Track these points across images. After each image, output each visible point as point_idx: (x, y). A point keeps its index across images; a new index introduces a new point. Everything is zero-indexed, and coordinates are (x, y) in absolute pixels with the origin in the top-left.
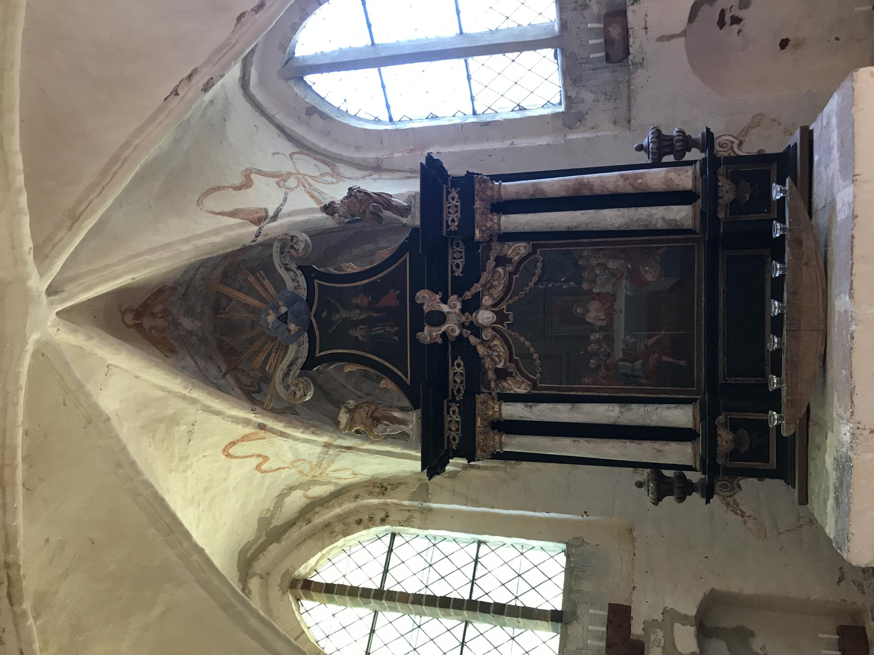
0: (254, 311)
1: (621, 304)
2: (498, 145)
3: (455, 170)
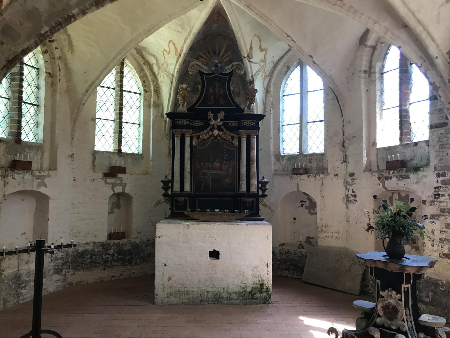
0: (219, 53)
1: (219, 172)
2: (272, 134)
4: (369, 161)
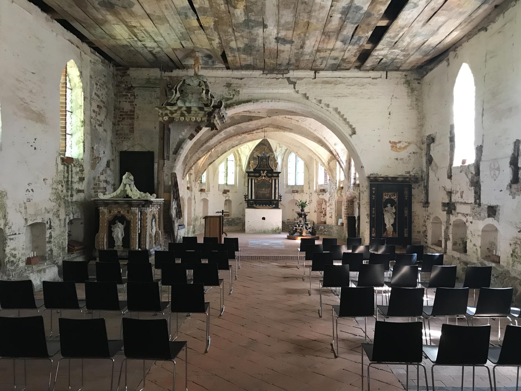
3: (280, 175)
4: (316, 189)
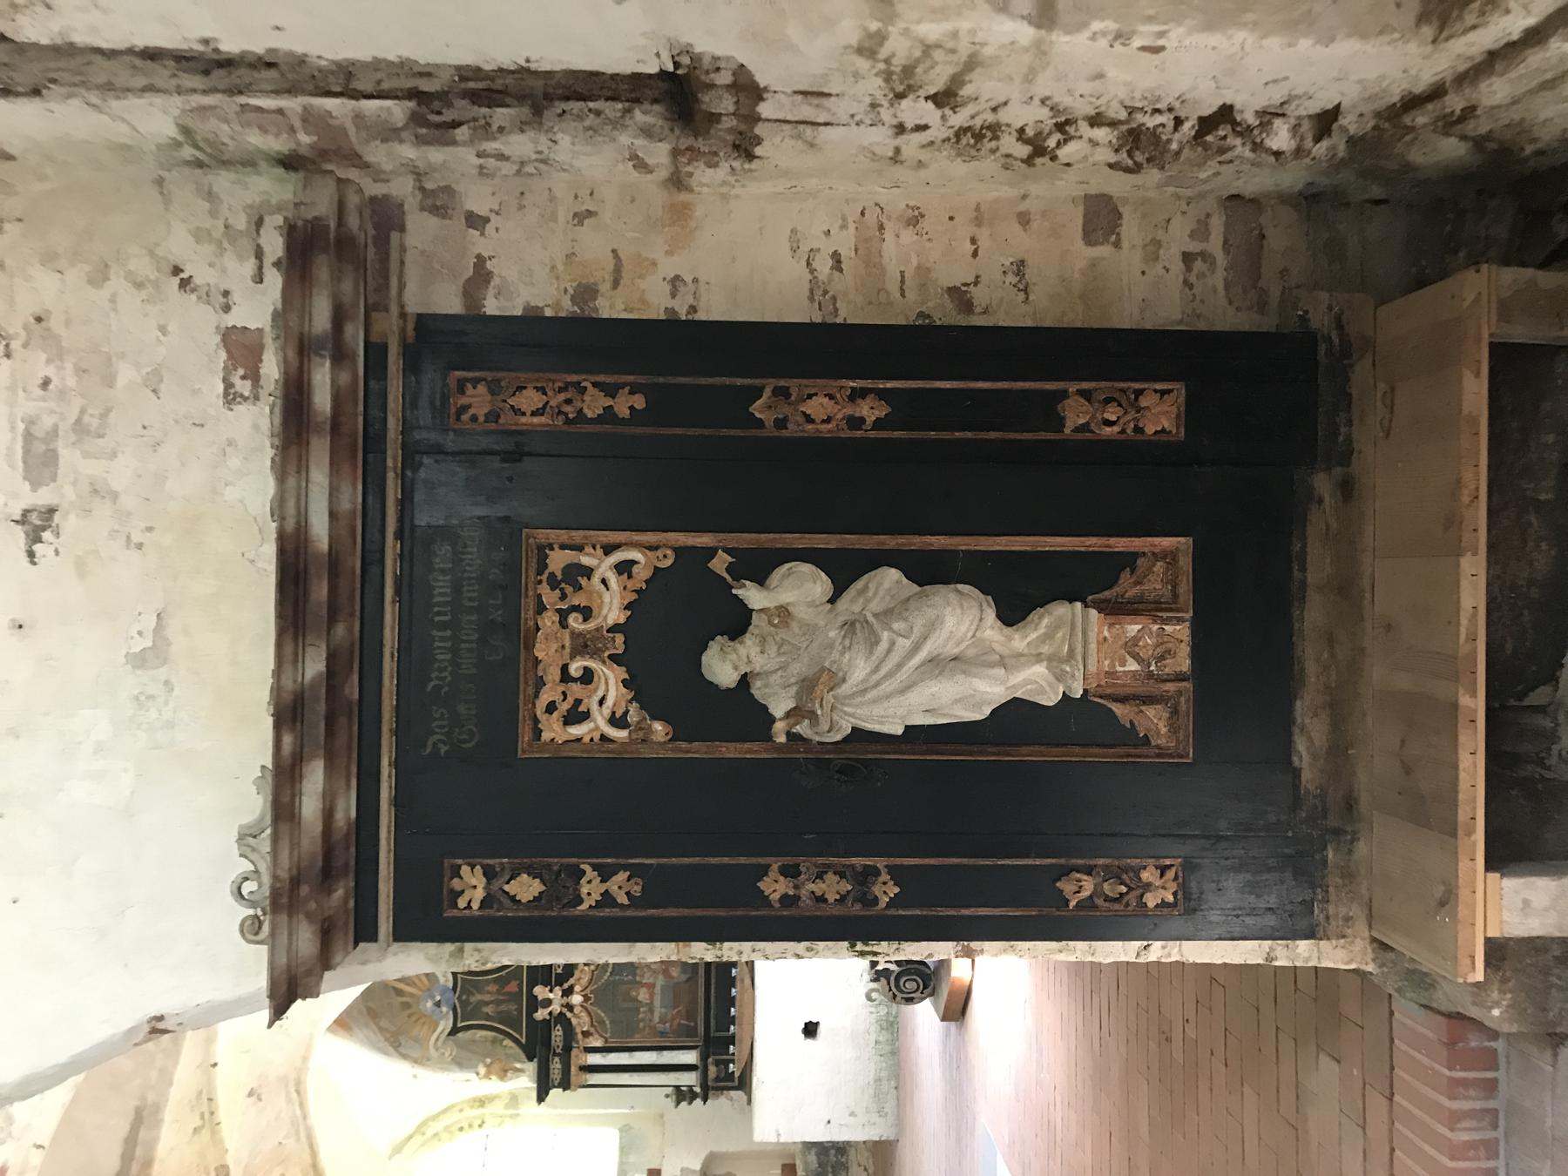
1: (658, 989)
